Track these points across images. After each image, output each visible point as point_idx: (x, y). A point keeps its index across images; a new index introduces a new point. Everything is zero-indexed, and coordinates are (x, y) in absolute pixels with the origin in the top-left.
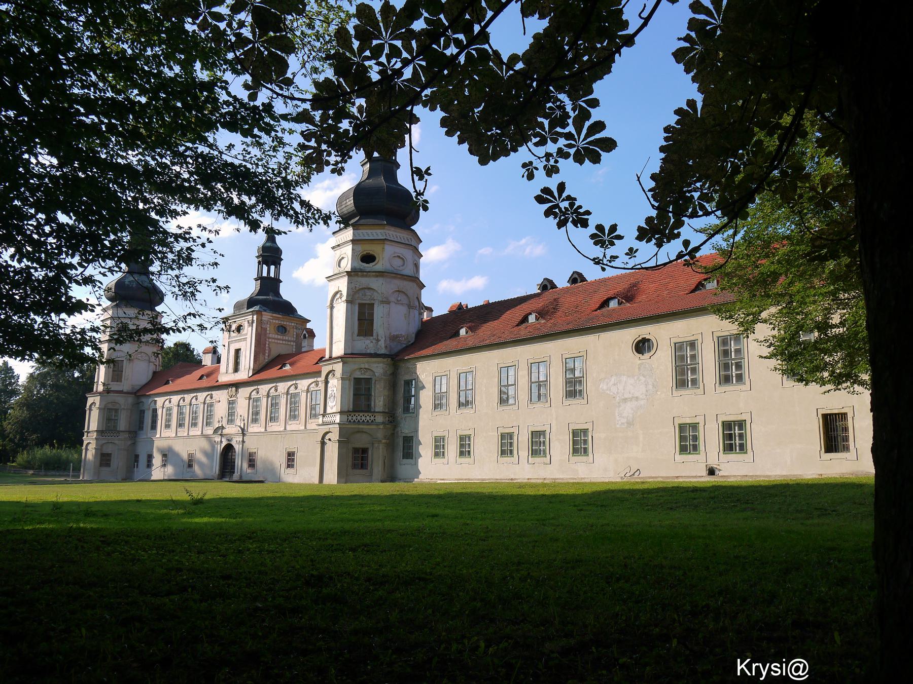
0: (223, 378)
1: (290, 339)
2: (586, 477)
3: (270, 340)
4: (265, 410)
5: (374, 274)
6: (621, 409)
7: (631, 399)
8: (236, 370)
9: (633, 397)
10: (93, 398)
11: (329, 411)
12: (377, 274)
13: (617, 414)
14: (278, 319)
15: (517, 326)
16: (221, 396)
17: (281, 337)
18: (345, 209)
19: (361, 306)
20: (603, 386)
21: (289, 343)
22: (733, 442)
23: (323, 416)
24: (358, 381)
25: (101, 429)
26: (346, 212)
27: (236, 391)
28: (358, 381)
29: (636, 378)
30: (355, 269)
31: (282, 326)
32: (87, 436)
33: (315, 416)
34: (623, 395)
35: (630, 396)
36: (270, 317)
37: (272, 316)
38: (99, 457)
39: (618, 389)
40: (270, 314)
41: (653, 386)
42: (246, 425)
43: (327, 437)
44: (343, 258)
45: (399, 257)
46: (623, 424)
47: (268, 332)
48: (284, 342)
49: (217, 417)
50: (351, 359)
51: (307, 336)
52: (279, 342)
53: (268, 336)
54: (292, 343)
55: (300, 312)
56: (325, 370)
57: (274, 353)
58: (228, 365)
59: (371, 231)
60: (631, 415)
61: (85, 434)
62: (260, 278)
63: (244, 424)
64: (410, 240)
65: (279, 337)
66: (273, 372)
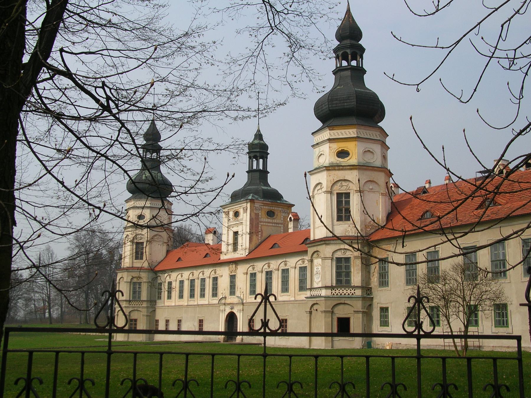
1: (278, 222)
3: (262, 224)
5: (348, 167)
16: (224, 273)
17: (271, 221)
19: (339, 195)
21: (278, 225)
36: (261, 204)
42: (245, 295)
43: (315, 307)
45: (369, 151)
47: (260, 216)
48: (273, 225)
51: (292, 219)
52: (269, 224)
54: (280, 225)
55: (285, 198)
65: (269, 220)
66: (265, 250)
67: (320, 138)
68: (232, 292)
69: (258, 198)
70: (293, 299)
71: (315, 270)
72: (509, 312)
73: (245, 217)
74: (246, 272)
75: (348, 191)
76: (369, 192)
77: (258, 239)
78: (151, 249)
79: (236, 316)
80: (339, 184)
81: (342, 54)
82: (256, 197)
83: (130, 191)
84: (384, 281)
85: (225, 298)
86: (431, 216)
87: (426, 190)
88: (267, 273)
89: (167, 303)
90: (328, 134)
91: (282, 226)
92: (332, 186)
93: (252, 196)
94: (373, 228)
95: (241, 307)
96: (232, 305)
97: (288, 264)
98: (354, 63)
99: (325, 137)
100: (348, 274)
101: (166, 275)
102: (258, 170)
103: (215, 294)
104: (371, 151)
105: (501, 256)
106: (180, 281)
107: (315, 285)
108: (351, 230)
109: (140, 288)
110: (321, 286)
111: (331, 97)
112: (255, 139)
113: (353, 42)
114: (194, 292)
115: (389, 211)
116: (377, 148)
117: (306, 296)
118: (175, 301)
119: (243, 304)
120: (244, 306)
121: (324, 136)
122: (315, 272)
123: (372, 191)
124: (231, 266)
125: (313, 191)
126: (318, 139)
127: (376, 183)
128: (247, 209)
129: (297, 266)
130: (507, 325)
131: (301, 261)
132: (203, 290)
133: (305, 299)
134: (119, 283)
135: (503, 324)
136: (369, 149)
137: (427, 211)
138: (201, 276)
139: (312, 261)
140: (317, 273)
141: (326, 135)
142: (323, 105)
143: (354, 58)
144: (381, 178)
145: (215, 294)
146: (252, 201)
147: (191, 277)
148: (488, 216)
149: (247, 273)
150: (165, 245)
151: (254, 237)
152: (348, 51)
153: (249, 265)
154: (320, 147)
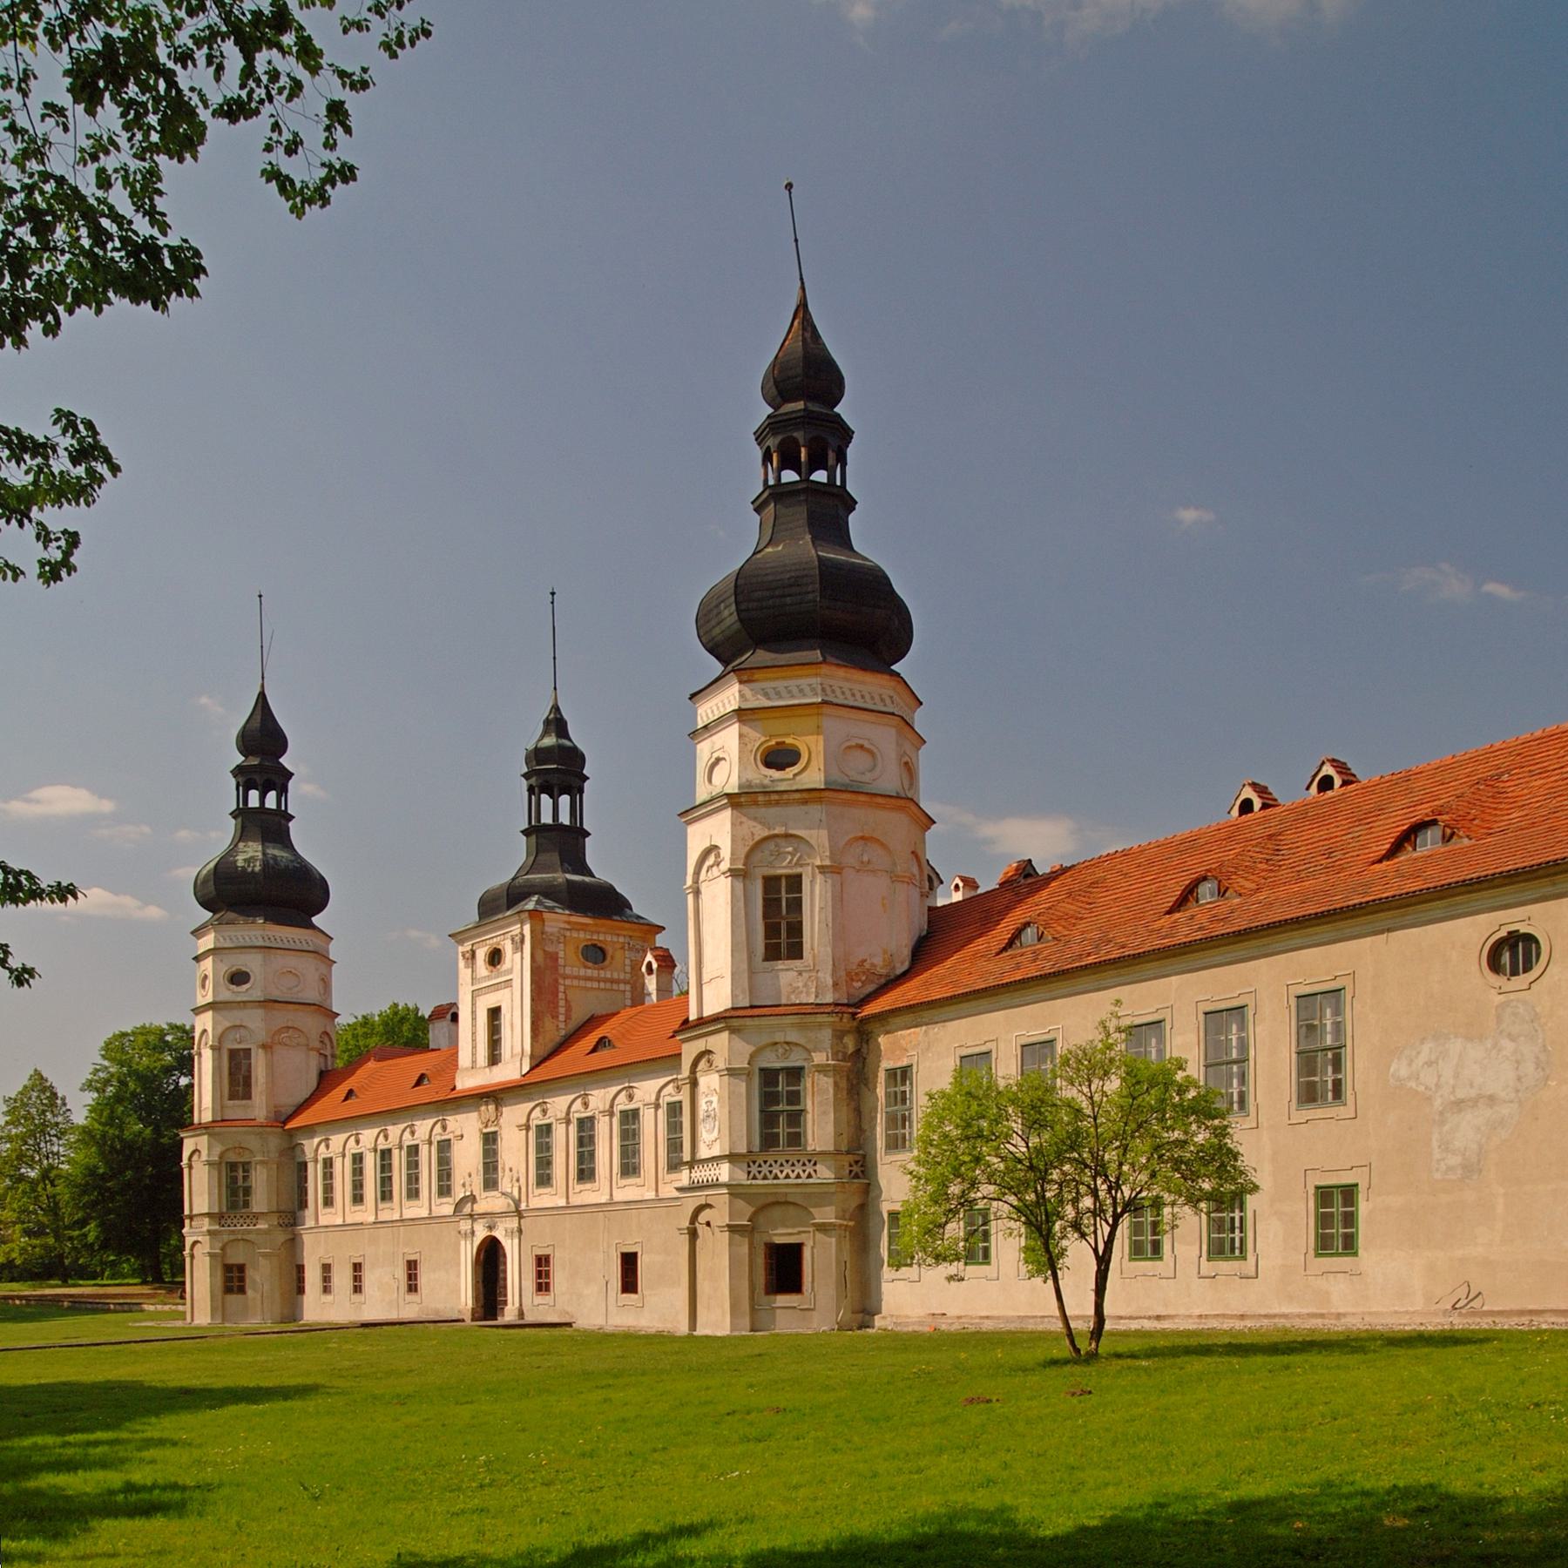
0: (466, 1081)
1: (615, 976)
2: (1350, 1310)
3: (568, 982)
4: (564, 1154)
5: (797, 796)
6: (1446, 1128)
7: (1475, 1102)
8: (494, 1059)
9: (1480, 1097)
10: (193, 1140)
11: (703, 1153)
12: (805, 795)
13: (1435, 1144)
14: (584, 927)
15: (1169, 913)
16: (466, 1127)
17: (595, 973)
18: (717, 631)
19: (771, 883)
20: (1400, 1068)
21: (615, 987)
22: (1142, 1050)
23: (691, 1168)
24: (769, 1076)
25: (216, 1211)
26: (720, 637)
27: (497, 1109)
28: (769, 1076)
29: (1489, 1043)
30: (750, 786)
31: (595, 946)
32: (191, 1226)
33: (674, 1166)
34: (1453, 1092)
35: (1473, 1093)
36: (563, 925)
37: (569, 923)
38: (219, 1273)
39: (1439, 1076)
40: (565, 918)
41: (1538, 1065)
42: (524, 1189)
43: (703, 1218)
44: (718, 760)
45: (862, 747)
46: (1450, 1169)
47: (561, 962)
48: (602, 985)
49: (458, 1178)
50: (748, 1022)
51: (655, 966)
52: (589, 984)
53: (561, 971)
54: (622, 987)
55: (637, 910)
56: (689, 1051)
57: (579, 1016)
58: (474, 1047)
59: (786, 683)
60: (1474, 1146)
61: (187, 1222)
62: (534, 831)
63: (520, 1188)
64: (888, 701)
65: (589, 973)
66: (577, 1056)
67: (715, 708)
68: (490, 1183)
69: (553, 907)
70: (651, 1195)
71: (702, 1106)
72: (1249, 1215)
73: (518, 964)
74: (524, 1121)
75: (798, 870)
76: (858, 871)
77: (558, 1029)
78: (270, 1067)
79: (503, 1248)
80: (771, 845)
81: (781, 444)
82: (550, 903)
83: (206, 904)
84: (900, 1137)
85: (472, 1199)
86: (1039, 940)
87: (1032, 872)
88: (581, 1122)
89: (329, 1217)
90: (737, 695)
91: (628, 987)
92: (748, 856)
93: (538, 902)
94: (872, 982)
95: (513, 1223)
96: (491, 1217)
97: (638, 1094)
98: (820, 476)
99: (727, 705)
100: (796, 1118)
101: (316, 1140)
102: (556, 827)
103: (445, 1190)
104: (867, 745)
105: (1234, 1051)
106: (354, 1156)
107: (703, 1153)
108: (805, 985)
109: (245, 1178)
110: (718, 1154)
111: (746, 586)
112: (545, 733)
113: (815, 407)
114: (391, 1186)
115: (922, 930)
116: (884, 737)
117: (679, 1185)
118: (341, 1212)
119: (519, 1214)
120: (522, 1221)
121: (726, 701)
122: (701, 1114)
123: (870, 867)
124: (483, 1108)
125: (697, 873)
126: (709, 711)
127: (882, 845)
128: (522, 941)
129: (661, 1101)
130: (1241, 1253)
131: (671, 1085)
132: (413, 1179)
133: (676, 1194)
134: (190, 1167)
135: (1233, 1249)
136: (861, 742)
137: (1027, 925)
138: (408, 1140)
139: (694, 1083)
140: (708, 1116)
141: (732, 698)
142: (722, 605)
143: (817, 462)
144: (894, 825)
145: (445, 1190)
146: (534, 914)
147: (382, 1145)
148: (1200, 929)
149: (528, 1128)
150: (314, 1054)
151: (548, 1023)
152: (799, 435)
153: (532, 1104)
154: (714, 738)
